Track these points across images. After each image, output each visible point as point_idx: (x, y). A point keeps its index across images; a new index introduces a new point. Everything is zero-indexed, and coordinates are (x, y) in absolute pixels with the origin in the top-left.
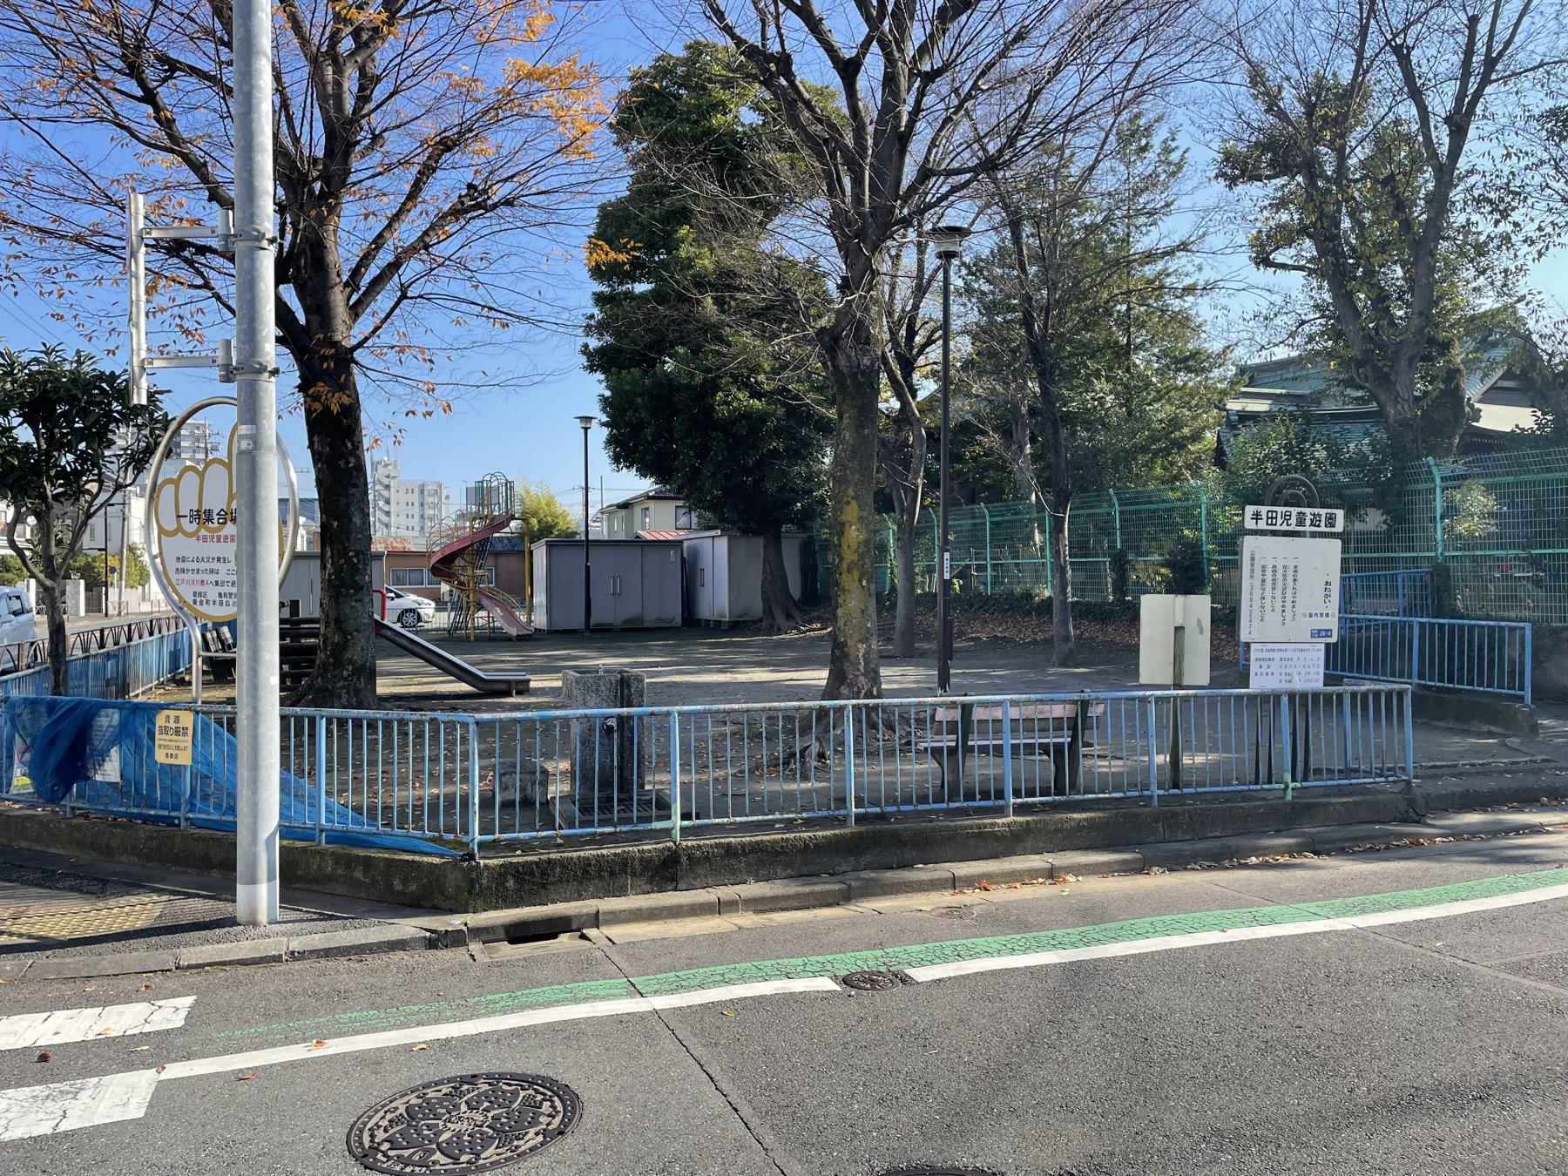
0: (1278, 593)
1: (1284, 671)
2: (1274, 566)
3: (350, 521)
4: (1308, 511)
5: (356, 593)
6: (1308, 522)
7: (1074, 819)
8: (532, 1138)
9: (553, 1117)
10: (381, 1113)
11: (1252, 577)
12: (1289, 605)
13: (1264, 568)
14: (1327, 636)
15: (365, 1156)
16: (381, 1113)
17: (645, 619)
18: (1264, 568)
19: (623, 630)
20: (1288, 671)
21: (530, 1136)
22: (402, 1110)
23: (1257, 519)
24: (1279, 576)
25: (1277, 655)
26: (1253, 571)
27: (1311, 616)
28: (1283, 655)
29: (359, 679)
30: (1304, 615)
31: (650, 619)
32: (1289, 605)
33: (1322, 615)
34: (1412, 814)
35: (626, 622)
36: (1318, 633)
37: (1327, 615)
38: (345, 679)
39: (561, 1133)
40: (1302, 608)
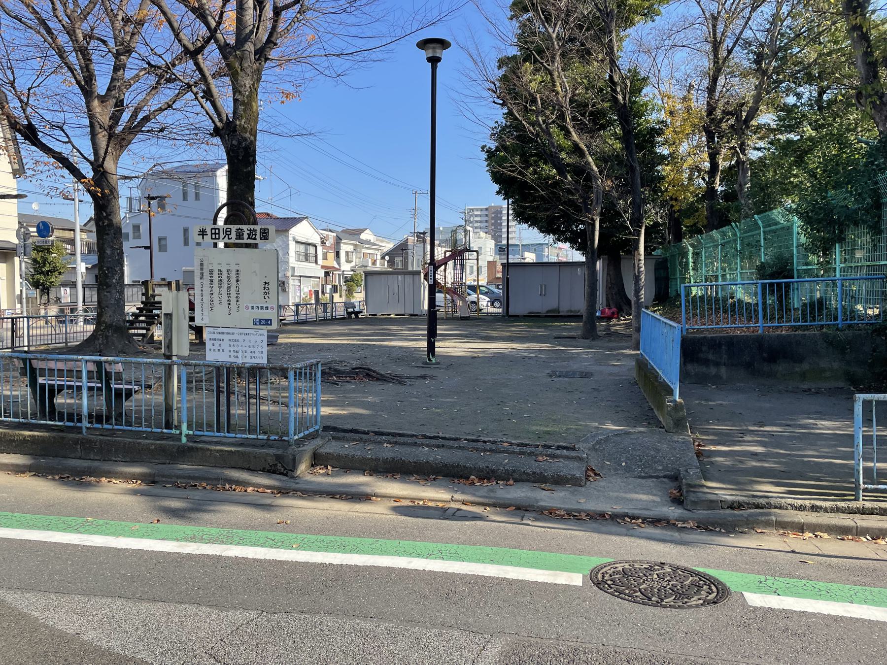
0: (224, 291)
1: (232, 349)
2: (220, 270)
3: (105, 252)
4: (245, 227)
5: (107, 287)
6: (246, 236)
7: (22, 435)
8: (694, 601)
9: (710, 594)
10: (609, 567)
11: (202, 278)
12: (233, 299)
13: (211, 272)
14: (267, 324)
15: (599, 584)
16: (609, 567)
17: (561, 309)
18: (211, 272)
19: (546, 316)
20: (236, 349)
21: (694, 599)
22: (620, 569)
23: (203, 235)
24: (224, 277)
25: (226, 337)
26: (202, 274)
27: (252, 308)
28: (231, 337)
29: (108, 331)
30: (247, 308)
31: (564, 309)
32: (233, 299)
33: (262, 308)
34: (279, 466)
35: (548, 311)
36: (260, 322)
37: (267, 308)
38: (102, 331)
39: (715, 603)
40: (245, 302)
